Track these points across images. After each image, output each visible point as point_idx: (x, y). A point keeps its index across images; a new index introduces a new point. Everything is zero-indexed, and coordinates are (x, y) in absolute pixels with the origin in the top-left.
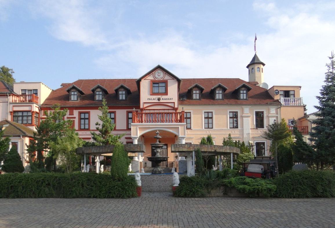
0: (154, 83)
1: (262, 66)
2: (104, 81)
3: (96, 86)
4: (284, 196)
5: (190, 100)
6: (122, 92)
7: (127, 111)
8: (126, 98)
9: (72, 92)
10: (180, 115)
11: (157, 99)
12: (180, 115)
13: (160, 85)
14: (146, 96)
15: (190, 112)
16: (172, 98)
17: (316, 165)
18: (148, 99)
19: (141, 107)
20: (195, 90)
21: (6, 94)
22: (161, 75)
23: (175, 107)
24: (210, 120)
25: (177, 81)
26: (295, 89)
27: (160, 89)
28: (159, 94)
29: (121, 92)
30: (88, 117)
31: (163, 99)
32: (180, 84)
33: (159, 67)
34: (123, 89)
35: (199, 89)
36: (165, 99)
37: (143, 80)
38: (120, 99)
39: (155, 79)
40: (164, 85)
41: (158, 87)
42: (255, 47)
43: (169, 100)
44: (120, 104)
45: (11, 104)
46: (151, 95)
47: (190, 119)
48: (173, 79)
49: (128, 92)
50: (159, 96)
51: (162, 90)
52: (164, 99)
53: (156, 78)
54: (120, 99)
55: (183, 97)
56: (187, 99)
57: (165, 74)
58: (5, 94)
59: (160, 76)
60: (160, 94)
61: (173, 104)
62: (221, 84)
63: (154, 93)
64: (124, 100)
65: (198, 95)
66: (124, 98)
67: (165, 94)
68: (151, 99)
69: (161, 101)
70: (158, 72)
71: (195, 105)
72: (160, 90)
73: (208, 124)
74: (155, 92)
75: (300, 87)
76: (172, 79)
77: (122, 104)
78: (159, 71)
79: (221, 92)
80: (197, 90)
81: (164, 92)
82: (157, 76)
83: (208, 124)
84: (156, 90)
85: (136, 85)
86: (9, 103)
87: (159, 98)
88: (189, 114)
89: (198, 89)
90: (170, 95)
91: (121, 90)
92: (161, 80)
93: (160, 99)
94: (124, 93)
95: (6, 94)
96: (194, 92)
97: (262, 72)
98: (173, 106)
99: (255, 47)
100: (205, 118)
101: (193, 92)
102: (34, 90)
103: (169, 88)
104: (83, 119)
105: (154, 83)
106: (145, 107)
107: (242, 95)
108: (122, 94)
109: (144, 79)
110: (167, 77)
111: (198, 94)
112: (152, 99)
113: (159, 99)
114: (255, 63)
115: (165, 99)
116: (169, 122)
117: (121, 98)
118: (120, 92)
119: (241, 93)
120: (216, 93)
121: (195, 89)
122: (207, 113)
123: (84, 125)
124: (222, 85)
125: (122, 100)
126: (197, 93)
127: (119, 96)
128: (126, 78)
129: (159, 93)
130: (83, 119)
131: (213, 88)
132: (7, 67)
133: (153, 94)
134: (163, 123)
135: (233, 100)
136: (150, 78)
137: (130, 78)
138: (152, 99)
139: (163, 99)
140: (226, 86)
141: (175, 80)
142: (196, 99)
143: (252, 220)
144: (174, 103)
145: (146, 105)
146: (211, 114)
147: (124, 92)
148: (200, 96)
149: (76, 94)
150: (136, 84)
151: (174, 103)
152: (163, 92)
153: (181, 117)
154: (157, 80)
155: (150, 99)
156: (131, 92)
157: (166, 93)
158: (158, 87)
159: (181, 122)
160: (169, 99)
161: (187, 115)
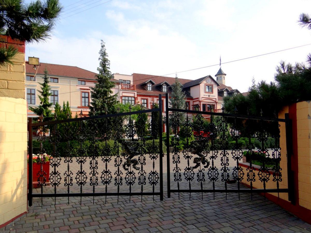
1: (224, 76)
17: (180, 130)
24: (33, 96)
30: (87, 96)
42: (220, 60)
47: (34, 96)
50: (209, 94)
69: (210, 97)
73: (31, 98)
83: (31, 98)
99: (220, 60)
100: (28, 94)
104: (87, 97)
113: (209, 96)
114: (220, 73)
121: (149, 83)
122: (84, 93)
123: (30, 100)
130: (87, 97)
132: (257, 83)
144: (216, 99)
145: (203, 99)
146: (87, 94)
161: (84, 95)
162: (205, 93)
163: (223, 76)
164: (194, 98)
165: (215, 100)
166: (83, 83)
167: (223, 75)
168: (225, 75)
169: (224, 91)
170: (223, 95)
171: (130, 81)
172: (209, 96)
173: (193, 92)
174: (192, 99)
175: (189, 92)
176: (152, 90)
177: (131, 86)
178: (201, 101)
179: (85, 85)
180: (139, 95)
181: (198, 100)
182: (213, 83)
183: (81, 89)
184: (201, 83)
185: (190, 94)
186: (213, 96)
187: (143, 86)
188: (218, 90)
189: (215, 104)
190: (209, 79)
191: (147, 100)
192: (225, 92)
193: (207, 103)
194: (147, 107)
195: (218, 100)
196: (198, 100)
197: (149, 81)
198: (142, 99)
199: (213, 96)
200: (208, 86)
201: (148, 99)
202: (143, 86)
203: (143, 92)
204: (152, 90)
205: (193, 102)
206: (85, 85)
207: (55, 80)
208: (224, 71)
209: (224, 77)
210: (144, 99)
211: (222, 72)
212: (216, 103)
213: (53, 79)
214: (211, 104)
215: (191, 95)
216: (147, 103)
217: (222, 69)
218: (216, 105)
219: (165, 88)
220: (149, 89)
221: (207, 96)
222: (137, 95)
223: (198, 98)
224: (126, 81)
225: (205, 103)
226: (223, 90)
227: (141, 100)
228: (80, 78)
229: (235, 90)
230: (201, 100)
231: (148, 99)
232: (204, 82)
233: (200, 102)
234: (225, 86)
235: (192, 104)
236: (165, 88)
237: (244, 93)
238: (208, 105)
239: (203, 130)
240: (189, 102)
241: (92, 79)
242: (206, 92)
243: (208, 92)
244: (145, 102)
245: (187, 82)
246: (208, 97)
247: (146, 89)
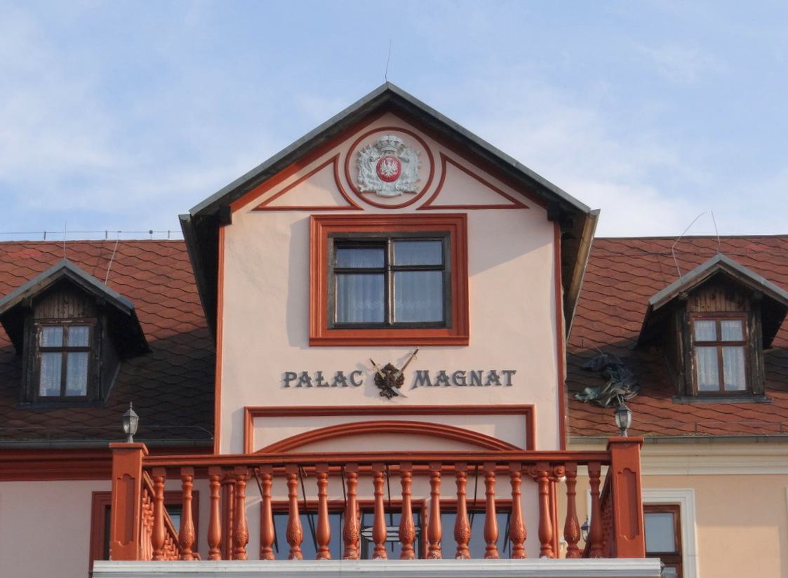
0: (342, 243)
2: (100, 251)
3: (44, 275)
5: (668, 403)
6: (65, 334)
8: (93, 380)
10: (594, 477)
11: (367, 377)
12: (594, 483)
13: (397, 254)
14: (269, 357)
15: (674, 509)
16: (510, 373)
18: (288, 378)
19: (226, 444)
20: (707, 316)
22: (406, 170)
23: (538, 447)
25: (550, 218)
27: (394, 290)
28: (383, 334)
29: (59, 331)
31: (422, 378)
32: (576, 250)
33: (391, 107)
34: (70, 311)
35: (740, 304)
36: (443, 379)
37: (242, 217)
38: (43, 393)
39: (354, 207)
40: (430, 253)
41: (384, 271)
43: (476, 389)
44: (43, 436)
46: (314, 342)
48: (518, 205)
49: (118, 331)
50: (393, 356)
51: (415, 299)
52: (433, 380)
53: (358, 194)
54: (43, 393)
55: (607, 379)
56: (640, 393)
57: (445, 159)
59: (397, 175)
60: (397, 334)
61: (518, 421)
63: (339, 327)
64: (76, 401)
65: (735, 361)
66: (78, 384)
67: (443, 333)
68: (320, 378)
69: (409, 395)
70: (378, 147)
71: (711, 440)
72: (396, 304)
74: (354, 318)
76: (511, 203)
77: (58, 436)
78: (393, 138)
80: (726, 316)
81: (439, 318)
82: (368, 179)
84: (360, 304)
85: (195, 288)
87: (389, 368)
88: (666, 520)
89: (732, 307)
90: (477, 354)
91: (55, 314)
92: (411, 210)
93: (400, 382)
94: (84, 342)
96: (703, 330)
101: (688, 330)
103: (478, 286)
105: (348, 241)
106: (256, 446)
108: (64, 350)
109: (257, 209)
110: (459, 190)
111: (740, 352)
112: (329, 378)
113: (387, 381)
115: (443, 379)
116: (488, 555)
117: (48, 385)
118: (48, 337)
120: (691, 347)
125: (63, 401)
126: (725, 338)
127: (39, 360)
128: (111, 237)
129: (386, 325)
133: (332, 332)
134: (421, 556)
136: (314, 192)
137: (147, 237)
138: (329, 378)
139: (422, 378)
141: (535, 213)
142: (721, 394)
144: (526, 412)
145: (266, 436)
147: (80, 335)
148: (758, 361)
150: (193, 279)
151: (526, 412)
152: (429, 319)
153: (604, 503)
154: (369, 210)
155: (305, 379)
156: (148, 338)
157: (452, 326)
158: (384, 271)
159: (612, 554)
160: (476, 379)
221: (340, 379)
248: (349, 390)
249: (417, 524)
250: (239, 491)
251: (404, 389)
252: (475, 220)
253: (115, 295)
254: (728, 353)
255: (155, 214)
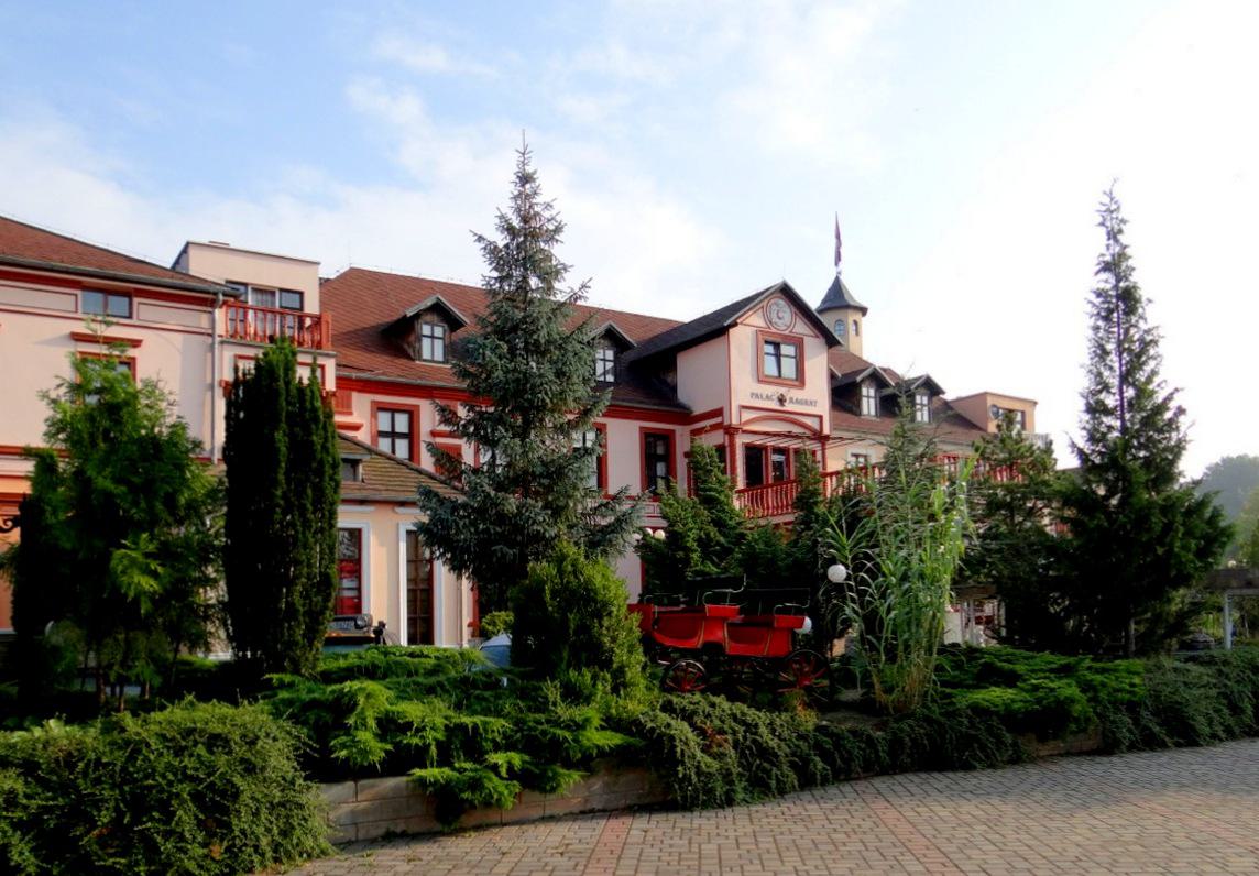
1: (857, 316)
4: (856, 765)
7: (641, 428)
9: (426, 323)
11: (775, 398)
21: (210, 296)
26: (1027, 409)
42: (838, 236)
45: (225, 346)
48: (817, 337)
50: (782, 390)
58: (208, 293)
62: (443, 300)
65: (439, 345)
69: (789, 407)
75: (1035, 403)
79: (438, 331)
86: (218, 339)
95: (210, 296)
97: (857, 332)
98: (817, 427)
99: (838, 236)
102: (282, 290)
104: (402, 436)
107: (426, 343)
113: (782, 400)
119: (435, 328)
120: (419, 338)
121: (428, 317)
124: (446, 302)
130: (402, 436)
131: (410, 313)
135: (387, 358)
140: (449, 301)
143: (933, 840)
144: (821, 417)
145: (747, 416)
149: (441, 335)
151: (821, 417)
162: (760, 381)
163: (852, 316)
164: (697, 411)
165: (813, 423)
166: (118, 303)
167: (850, 312)
168: (863, 311)
169: (862, 381)
170: (859, 405)
171: (301, 294)
172: (782, 400)
173: (693, 379)
174: (684, 416)
175: (669, 380)
176: (446, 361)
177: (308, 322)
178: (737, 429)
179: (130, 317)
180: (359, 380)
181: (718, 420)
182: (801, 328)
183: (77, 338)
184: (735, 324)
185: (674, 389)
186: (806, 403)
187: (396, 337)
188: (832, 376)
189: (816, 446)
190: (782, 302)
191: (413, 415)
192: (864, 391)
193: (771, 442)
194: (411, 458)
195: (834, 427)
196: (718, 420)
197: (429, 303)
198: (381, 408)
199: (806, 403)
200: (777, 346)
201: (418, 407)
202: (396, 337)
203: (384, 367)
204: (446, 361)
205: (695, 433)
206: (130, 317)
207: (113, 300)
208: (856, 292)
209: (856, 323)
210: (393, 410)
211: (846, 296)
212: (822, 438)
213: (100, 296)
214: (794, 444)
215: (683, 396)
216: (411, 436)
217: (845, 280)
218: (819, 456)
219: (868, 397)
220: (426, 354)
221: (768, 398)
222: (339, 378)
223: (718, 413)
224: (272, 293)
225: (757, 441)
226: (859, 379)
227: (374, 416)
228: (20, 259)
229: (917, 379)
230: (735, 422)
231: (418, 407)
232: (755, 319)
233: (731, 431)
234: (860, 359)
235: (687, 448)
236: (868, 397)
237: (960, 400)
238: (778, 450)
239: (735, 599)
240: (667, 438)
241: (123, 273)
242: (762, 379)
243: (779, 379)
244: (402, 424)
245: (659, 330)
246: (774, 405)
247: (410, 351)
248: (770, 402)
249: (124, 412)
250: (443, 416)
251: (786, 404)
252: (806, 339)
253: (630, 340)
254: (436, 341)
255: (684, 309)
